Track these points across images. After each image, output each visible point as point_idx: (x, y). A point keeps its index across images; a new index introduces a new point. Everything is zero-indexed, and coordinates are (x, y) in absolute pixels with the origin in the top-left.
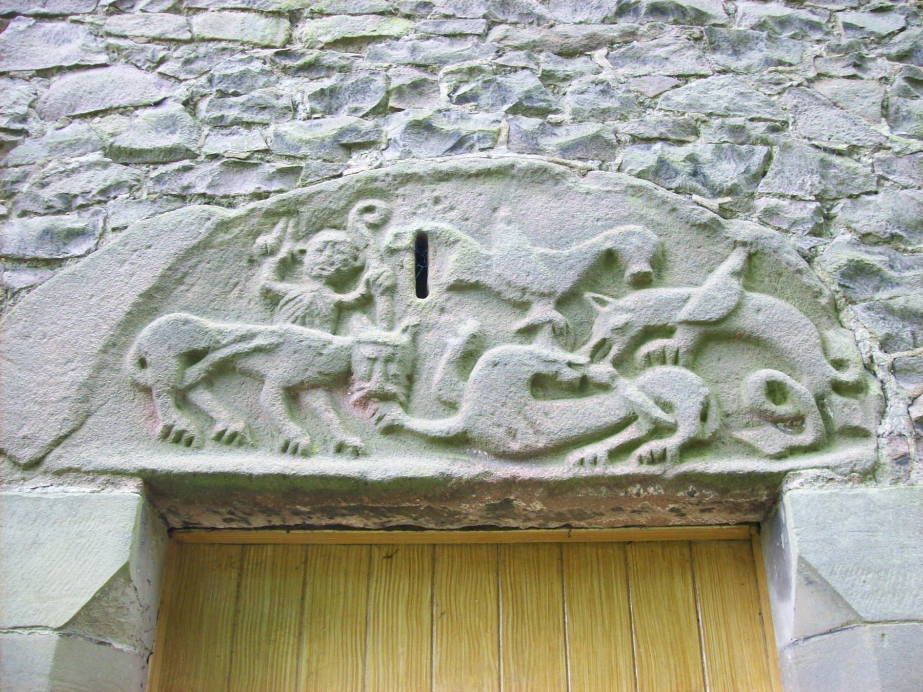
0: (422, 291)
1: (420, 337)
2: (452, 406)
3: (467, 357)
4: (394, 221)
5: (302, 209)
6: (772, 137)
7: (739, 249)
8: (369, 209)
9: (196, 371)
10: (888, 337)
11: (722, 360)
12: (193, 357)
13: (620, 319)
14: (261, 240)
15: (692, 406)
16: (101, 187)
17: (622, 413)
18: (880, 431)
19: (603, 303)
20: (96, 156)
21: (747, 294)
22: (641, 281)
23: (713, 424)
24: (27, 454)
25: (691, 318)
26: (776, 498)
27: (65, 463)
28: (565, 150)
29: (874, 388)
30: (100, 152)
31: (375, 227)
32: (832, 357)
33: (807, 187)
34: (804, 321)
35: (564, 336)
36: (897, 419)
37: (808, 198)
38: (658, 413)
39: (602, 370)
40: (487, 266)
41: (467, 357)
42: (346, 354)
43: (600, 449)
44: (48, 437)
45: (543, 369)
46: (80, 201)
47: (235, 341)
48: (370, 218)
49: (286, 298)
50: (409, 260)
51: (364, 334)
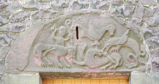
0: (78, 38)
1: (78, 47)
2: (83, 60)
3: (85, 51)
4: (73, 24)
5: (58, 22)
6: (136, 4)
7: (128, 29)
8: (68, 22)
9: (44, 54)
10: (150, 47)
11: (124, 51)
12: (43, 51)
13: (108, 44)
14: (51, 28)
15: (118, 60)
16: (23, 17)
17: (108, 61)
18: (147, 64)
19: (106, 41)
20: (21, 10)
21: (129, 38)
22: (112, 36)
23: (121, 63)
24: (21, 69)
25: (119, 44)
26: (130, 76)
27: (27, 70)
28: (100, 8)
29: (147, 56)
30: (22, 9)
31: (69, 25)
32: (141, 51)
33: (141, 15)
34: (137, 44)
35: (100, 47)
36: (149, 63)
37: (141, 18)
38: (113, 61)
39: (105, 53)
40: (88, 33)
41: (85, 51)
42: (67, 50)
43: (104, 67)
44: (24, 66)
45: (96, 53)
46: (20, 20)
47: (50, 48)
48: (69, 23)
49: (57, 40)
50: (75, 32)
51: (69, 47)
